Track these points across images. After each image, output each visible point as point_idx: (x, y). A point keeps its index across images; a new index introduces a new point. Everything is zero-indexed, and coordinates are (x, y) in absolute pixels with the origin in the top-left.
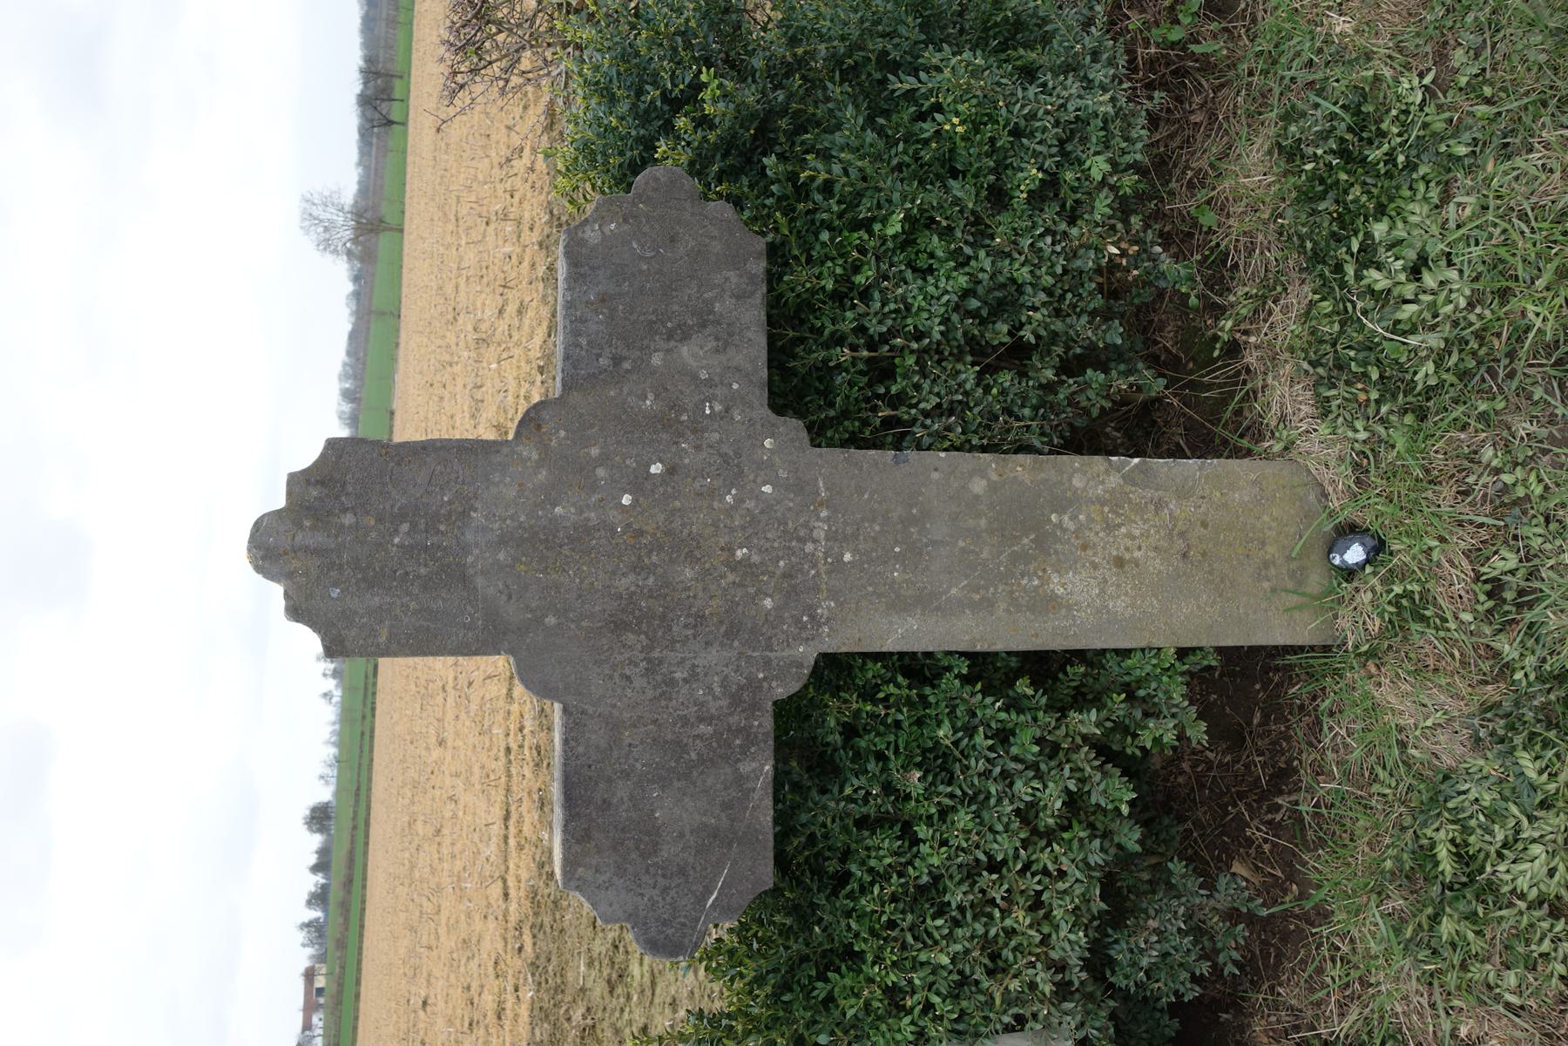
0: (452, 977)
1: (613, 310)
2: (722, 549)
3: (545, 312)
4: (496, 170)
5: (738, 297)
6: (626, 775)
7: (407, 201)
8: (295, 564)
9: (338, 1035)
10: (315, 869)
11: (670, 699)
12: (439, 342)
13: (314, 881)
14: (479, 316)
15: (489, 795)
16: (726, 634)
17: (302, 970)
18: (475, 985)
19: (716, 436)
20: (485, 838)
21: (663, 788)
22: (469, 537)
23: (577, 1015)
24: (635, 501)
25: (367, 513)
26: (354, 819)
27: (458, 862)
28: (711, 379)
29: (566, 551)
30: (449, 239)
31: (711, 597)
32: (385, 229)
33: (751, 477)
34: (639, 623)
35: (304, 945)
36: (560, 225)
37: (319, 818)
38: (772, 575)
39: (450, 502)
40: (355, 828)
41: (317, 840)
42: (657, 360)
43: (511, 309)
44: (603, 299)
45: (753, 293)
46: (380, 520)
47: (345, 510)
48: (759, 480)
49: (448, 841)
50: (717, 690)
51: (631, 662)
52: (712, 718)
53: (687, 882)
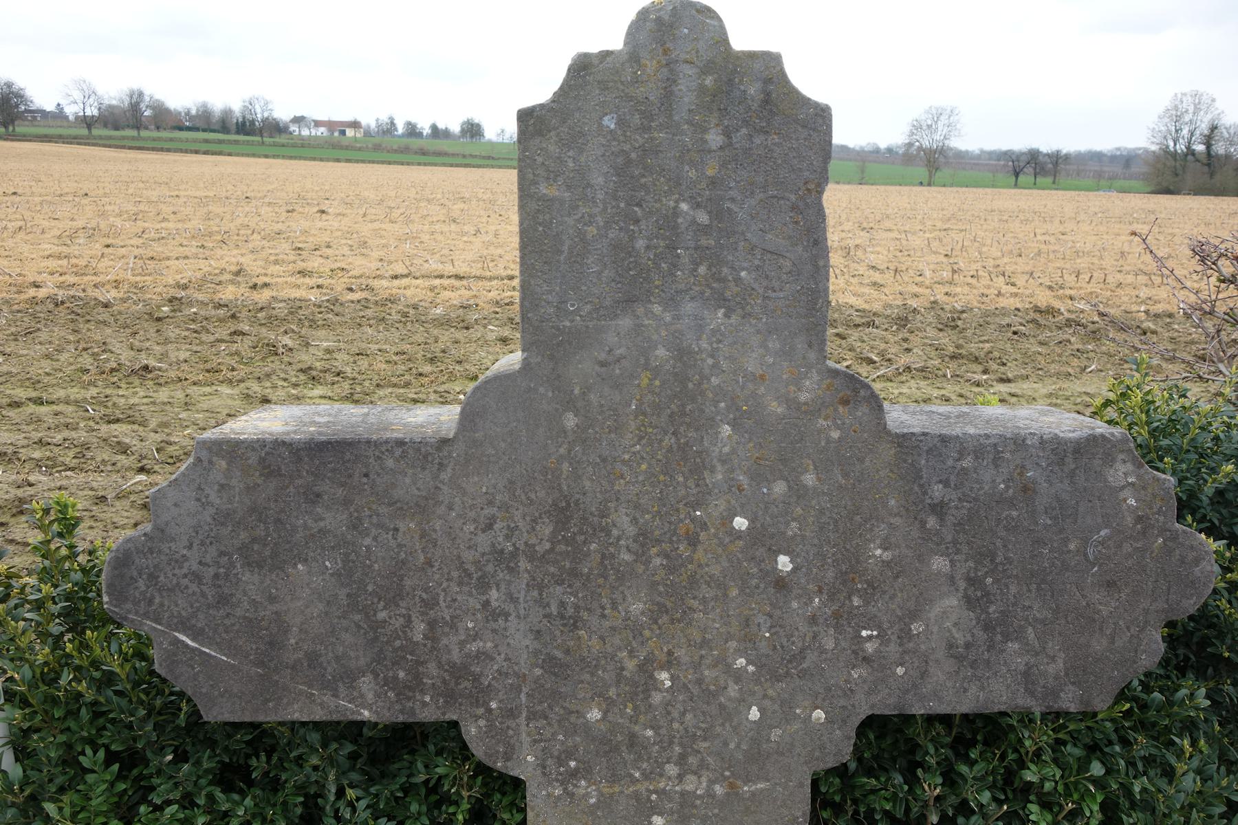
0: (339, 233)
1: (1011, 503)
2: (670, 653)
3: (877, 307)
4: (991, 263)
5: (1027, 674)
6: (355, 525)
7: (955, 189)
8: (651, 66)
9: (309, 146)
10: (434, 128)
11: (460, 584)
12: (844, 217)
13: (425, 126)
14: (869, 250)
15: (478, 262)
16: (551, 658)
17: (359, 119)
18: (329, 251)
19: (829, 644)
20: (444, 259)
21: (337, 574)
22: (689, 307)
23: (287, 340)
24: (739, 535)
25: (724, 165)
26: (471, 156)
27: (428, 237)
28: (910, 637)
29: (669, 440)
30: (929, 223)
31: (602, 638)
32: (930, 172)
33: (770, 692)
34: (566, 541)
35: (377, 120)
36: (954, 320)
37: (472, 130)
38: (634, 720)
39: (738, 280)
40: (464, 156)
41: (455, 128)
42: (939, 563)
43: (877, 277)
44: (1027, 489)
45: (1032, 694)
46: (713, 182)
47: (727, 133)
48: (767, 703)
49: (445, 228)
50: (473, 647)
51: (511, 532)
52: (435, 640)
53: (209, 607)
